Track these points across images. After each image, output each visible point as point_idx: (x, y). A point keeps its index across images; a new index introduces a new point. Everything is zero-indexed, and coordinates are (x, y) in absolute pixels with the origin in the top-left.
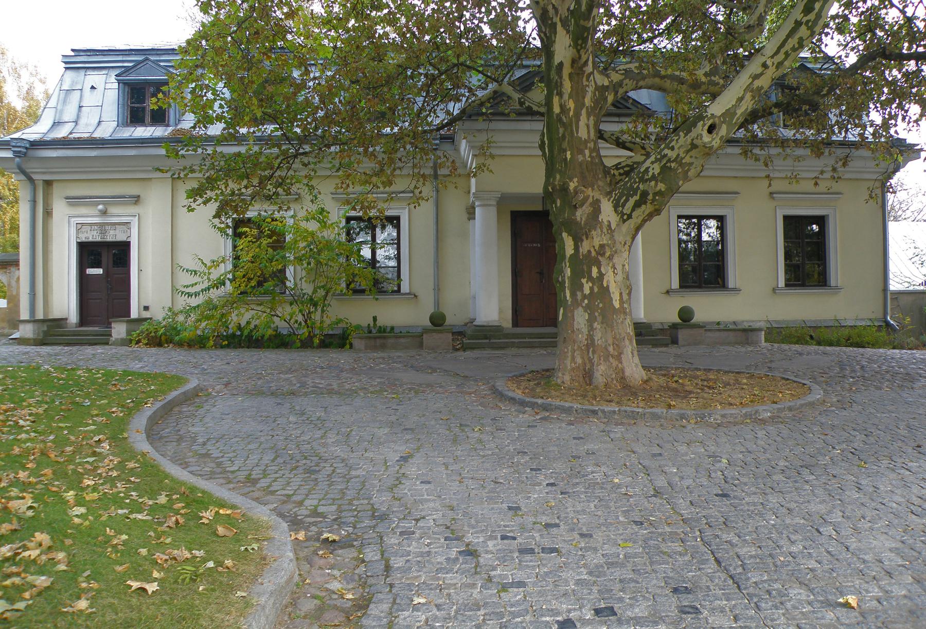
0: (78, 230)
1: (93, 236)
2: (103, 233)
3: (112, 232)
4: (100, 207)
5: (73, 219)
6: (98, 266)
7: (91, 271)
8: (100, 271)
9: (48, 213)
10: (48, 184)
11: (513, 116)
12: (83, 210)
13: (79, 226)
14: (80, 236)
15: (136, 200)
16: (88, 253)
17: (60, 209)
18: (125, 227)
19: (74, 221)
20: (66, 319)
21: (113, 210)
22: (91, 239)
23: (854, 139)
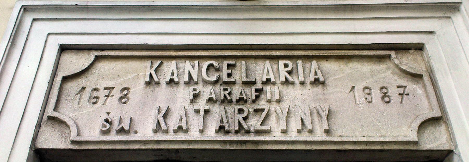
3: (299, 98)
18: (383, 74)
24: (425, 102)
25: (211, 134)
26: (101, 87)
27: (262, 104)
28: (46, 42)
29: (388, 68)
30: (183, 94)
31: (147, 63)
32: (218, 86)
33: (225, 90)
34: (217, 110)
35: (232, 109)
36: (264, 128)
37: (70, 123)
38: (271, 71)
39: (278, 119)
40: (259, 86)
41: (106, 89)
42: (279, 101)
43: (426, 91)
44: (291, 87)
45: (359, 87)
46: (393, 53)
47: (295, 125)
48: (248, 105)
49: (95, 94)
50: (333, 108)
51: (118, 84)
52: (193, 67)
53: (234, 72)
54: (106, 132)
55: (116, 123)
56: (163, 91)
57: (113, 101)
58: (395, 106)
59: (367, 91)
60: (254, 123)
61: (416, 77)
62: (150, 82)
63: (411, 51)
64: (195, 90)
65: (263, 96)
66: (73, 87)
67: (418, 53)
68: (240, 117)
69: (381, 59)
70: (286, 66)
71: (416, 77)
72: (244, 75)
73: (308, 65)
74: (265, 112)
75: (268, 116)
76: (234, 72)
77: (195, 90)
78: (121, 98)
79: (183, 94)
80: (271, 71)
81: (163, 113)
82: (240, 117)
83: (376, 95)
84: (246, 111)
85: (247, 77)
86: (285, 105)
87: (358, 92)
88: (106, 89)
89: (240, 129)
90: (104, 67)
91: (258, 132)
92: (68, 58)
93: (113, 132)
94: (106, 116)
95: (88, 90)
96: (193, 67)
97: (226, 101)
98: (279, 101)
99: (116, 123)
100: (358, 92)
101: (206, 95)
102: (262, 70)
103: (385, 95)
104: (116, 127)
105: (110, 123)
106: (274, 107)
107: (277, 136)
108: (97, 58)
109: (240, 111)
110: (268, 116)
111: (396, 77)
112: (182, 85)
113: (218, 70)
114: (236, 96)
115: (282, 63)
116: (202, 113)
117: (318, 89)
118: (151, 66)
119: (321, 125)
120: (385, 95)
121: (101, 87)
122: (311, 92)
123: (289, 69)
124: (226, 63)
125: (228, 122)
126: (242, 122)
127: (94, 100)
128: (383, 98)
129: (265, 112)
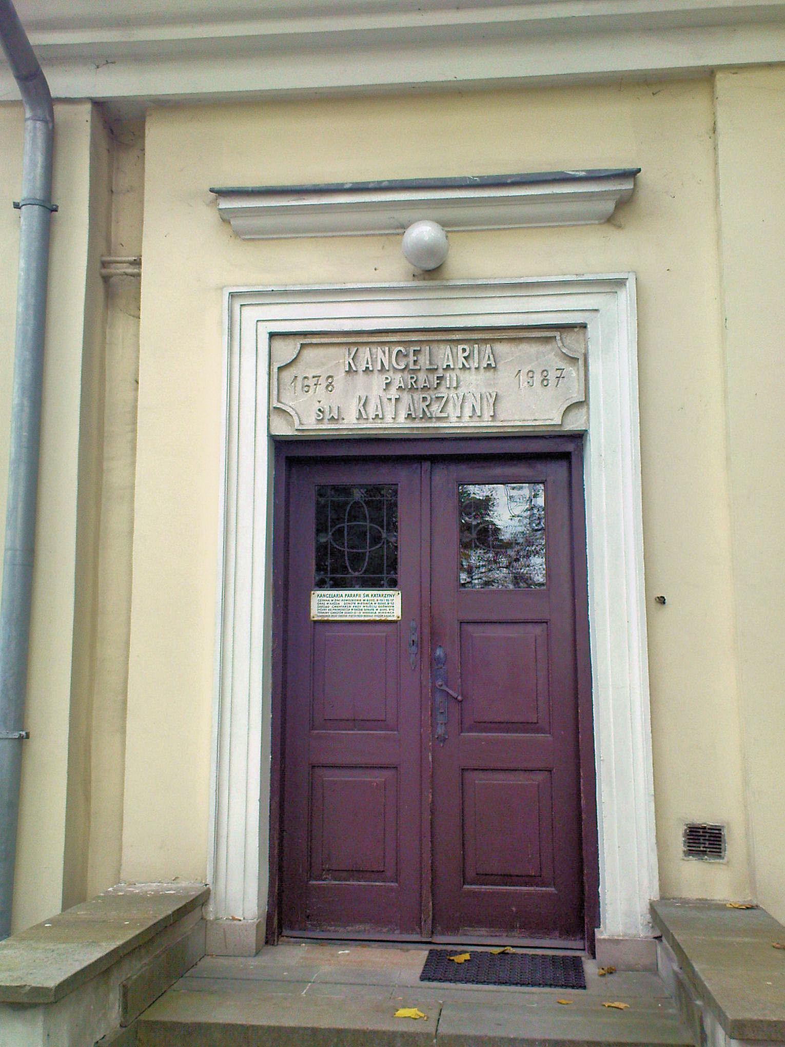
0: (279, 371)
1: (363, 403)
2: (426, 384)
3: (473, 383)
4: (424, 232)
5: (251, 315)
6: (380, 574)
7: (329, 604)
8: (385, 605)
9: (115, 285)
10: (120, 128)
11: (434, 420)
12: (309, 264)
13: (286, 351)
14: (289, 402)
15: (618, 196)
16: (336, 502)
17: (185, 261)
18: (546, 356)
19: (256, 321)
20: (201, 900)
21: (475, 259)
22: (351, 422)
23: (542, 494)
24: (576, 384)
25: (402, 417)
26: (310, 376)
27: (443, 392)
28: (269, 425)
29: (552, 350)
30: (378, 381)
31: (343, 350)
32: (406, 372)
33: (412, 378)
34: (406, 397)
35: (418, 396)
36: (443, 415)
37: (293, 413)
38: (450, 357)
39: (455, 405)
40: (440, 373)
41: (314, 377)
42: (456, 388)
43: (578, 375)
44: (467, 371)
45: (525, 371)
46: (557, 334)
47: (468, 411)
48: (431, 392)
49: (306, 382)
50: (500, 393)
51: (322, 372)
52: (384, 353)
53: (419, 357)
54: (320, 421)
55: (327, 411)
56: (361, 378)
57: (321, 389)
58: (551, 391)
59: (530, 374)
60: (435, 408)
61: (574, 360)
62: (350, 371)
63: (576, 330)
64: (387, 378)
65: (443, 382)
66: (287, 375)
67: (581, 332)
68: (424, 405)
69: (548, 340)
70: (464, 350)
71: (574, 360)
72: (428, 362)
73: (483, 348)
74: (445, 399)
75: (447, 402)
76: (419, 357)
77: (387, 378)
78: (328, 386)
79: (378, 381)
80: (450, 357)
81: (362, 402)
82: (424, 405)
83: (538, 378)
84: (429, 399)
85: (431, 364)
86: (462, 391)
87: (523, 377)
88: (314, 377)
89: (424, 417)
90: (309, 354)
91: (439, 419)
92: (278, 344)
93: (326, 421)
94: (317, 406)
95: (300, 379)
96: (384, 353)
97: (412, 389)
98: (456, 388)
99: (327, 411)
100: (523, 377)
101: (396, 385)
102: (444, 355)
103: (545, 379)
104: (328, 417)
105: (322, 412)
106: (452, 394)
107: (453, 422)
108: (303, 346)
109: (424, 399)
110: (447, 402)
111: (557, 359)
112: (376, 372)
113: (406, 356)
114: (421, 384)
115: (460, 347)
116: (393, 401)
117: (490, 374)
118: (350, 354)
119: (489, 412)
120: (545, 379)
121: (310, 376)
122: (483, 375)
123: (466, 354)
124: (412, 349)
125: (415, 410)
126: (426, 410)
127: (306, 389)
128: (542, 381)
129: (445, 399)
